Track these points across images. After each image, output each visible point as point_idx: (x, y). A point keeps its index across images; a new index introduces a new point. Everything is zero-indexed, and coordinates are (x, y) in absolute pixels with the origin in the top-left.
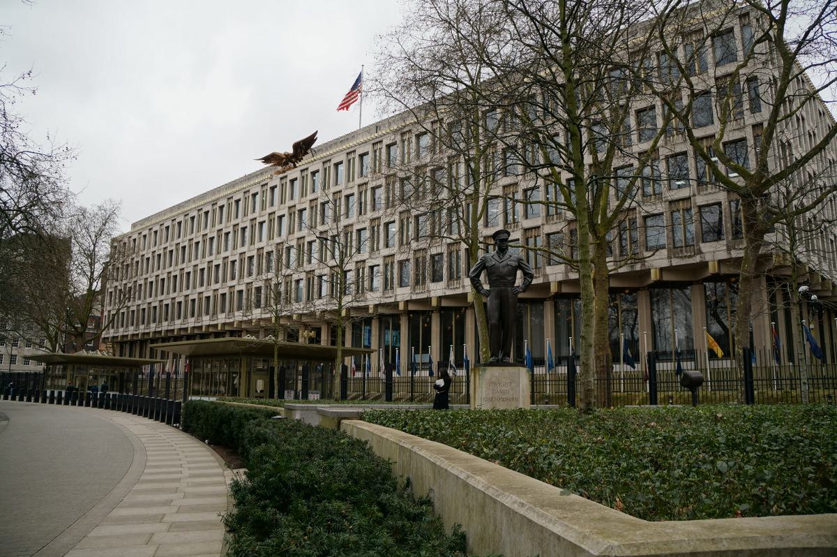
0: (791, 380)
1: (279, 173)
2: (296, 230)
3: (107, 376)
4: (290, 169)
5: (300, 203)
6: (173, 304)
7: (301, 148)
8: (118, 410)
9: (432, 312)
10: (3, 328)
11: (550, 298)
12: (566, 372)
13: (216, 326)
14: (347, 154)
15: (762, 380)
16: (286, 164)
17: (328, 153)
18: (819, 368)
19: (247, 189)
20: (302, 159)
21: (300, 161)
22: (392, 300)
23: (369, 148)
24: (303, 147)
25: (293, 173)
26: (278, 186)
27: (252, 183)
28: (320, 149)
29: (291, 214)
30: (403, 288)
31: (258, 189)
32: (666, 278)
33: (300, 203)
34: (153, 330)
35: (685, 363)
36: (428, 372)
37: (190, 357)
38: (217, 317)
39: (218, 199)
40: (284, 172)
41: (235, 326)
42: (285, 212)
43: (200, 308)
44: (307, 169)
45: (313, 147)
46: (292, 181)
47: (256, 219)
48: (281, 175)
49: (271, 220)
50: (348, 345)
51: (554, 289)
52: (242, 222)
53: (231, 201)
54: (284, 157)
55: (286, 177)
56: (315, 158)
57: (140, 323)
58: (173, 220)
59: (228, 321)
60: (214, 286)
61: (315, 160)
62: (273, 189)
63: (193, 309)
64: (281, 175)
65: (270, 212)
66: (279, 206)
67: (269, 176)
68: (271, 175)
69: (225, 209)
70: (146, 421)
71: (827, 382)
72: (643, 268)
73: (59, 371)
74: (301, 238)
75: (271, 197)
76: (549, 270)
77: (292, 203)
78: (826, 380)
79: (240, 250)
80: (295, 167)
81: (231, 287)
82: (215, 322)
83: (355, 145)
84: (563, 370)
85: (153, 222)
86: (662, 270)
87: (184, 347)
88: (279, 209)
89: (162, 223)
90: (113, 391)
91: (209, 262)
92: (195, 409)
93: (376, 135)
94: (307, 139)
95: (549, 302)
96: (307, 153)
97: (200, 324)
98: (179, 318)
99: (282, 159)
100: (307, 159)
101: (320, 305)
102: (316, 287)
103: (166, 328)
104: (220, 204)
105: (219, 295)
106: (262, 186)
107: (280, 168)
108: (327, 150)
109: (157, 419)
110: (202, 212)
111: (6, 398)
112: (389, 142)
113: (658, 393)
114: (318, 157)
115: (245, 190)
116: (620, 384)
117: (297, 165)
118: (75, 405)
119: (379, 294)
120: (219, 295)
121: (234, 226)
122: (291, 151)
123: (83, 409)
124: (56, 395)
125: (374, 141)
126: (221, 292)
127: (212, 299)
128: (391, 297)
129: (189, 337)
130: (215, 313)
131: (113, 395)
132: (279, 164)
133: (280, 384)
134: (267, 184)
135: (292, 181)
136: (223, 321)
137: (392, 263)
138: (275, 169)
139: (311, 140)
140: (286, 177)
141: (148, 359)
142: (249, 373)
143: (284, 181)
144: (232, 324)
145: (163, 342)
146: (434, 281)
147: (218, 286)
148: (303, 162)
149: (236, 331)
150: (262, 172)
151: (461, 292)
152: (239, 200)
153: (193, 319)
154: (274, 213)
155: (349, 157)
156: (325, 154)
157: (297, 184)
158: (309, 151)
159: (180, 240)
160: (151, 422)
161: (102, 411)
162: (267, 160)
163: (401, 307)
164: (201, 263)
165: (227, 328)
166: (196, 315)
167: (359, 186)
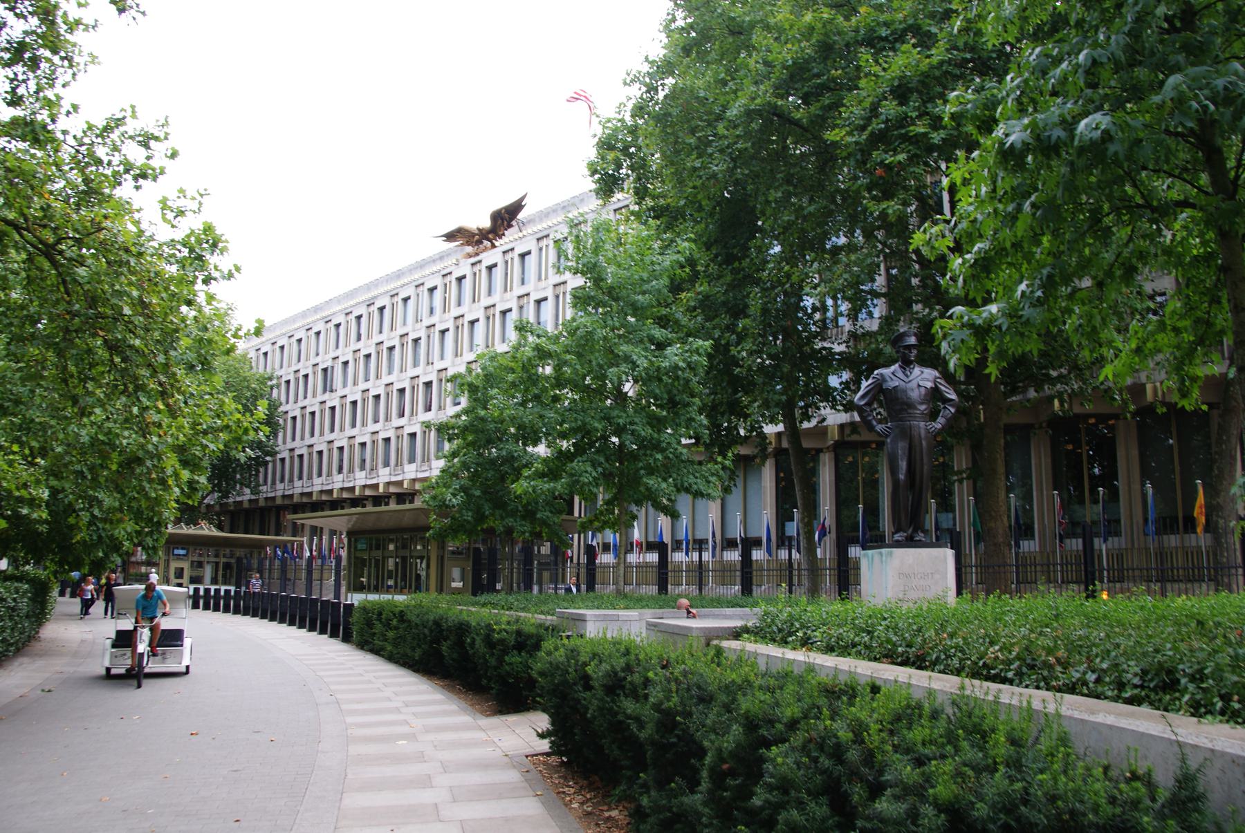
1: (470, 256)
2: (464, 351)
3: (217, 564)
4: (486, 249)
5: (502, 300)
6: (310, 454)
7: (502, 219)
8: (263, 617)
11: (828, 448)
13: (376, 486)
16: (479, 242)
17: (545, 226)
19: (420, 282)
20: (504, 234)
21: (500, 238)
24: (505, 218)
25: (489, 257)
27: (428, 272)
28: (531, 221)
29: (488, 318)
31: (437, 281)
33: (502, 300)
34: (279, 493)
36: (1080, 541)
37: (349, 534)
38: (377, 473)
39: (376, 297)
40: (477, 254)
41: (405, 486)
42: (480, 314)
43: (310, 467)
44: (512, 249)
45: (521, 216)
46: (490, 268)
47: (434, 325)
48: (473, 260)
49: (458, 327)
51: (834, 435)
52: (414, 331)
53: (395, 299)
54: (477, 232)
55: (480, 262)
56: (525, 233)
58: (308, 330)
59: (394, 479)
60: (397, 422)
61: (524, 236)
62: (460, 280)
63: (341, 460)
64: (473, 260)
65: (429, 324)
66: (413, 325)
67: (454, 261)
68: (457, 260)
69: (387, 312)
70: (293, 631)
73: (525, 526)
75: (457, 292)
77: (489, 302)
79: (412, 372)
80: (494, 246)
81: (350, 438)
82: (374, 481)
84: (1076, 544)
85: (278, 333)
87: (339, 521)
88: (470, 311)
89: (347, 311)
90: (225, 583)
91: (363, 391)
92: (372, 616)
93: (521, 235)
94: (511, 205)
95: (827, 455)
96: (510, 226)
97: (351, 485)
99: (473, 235)
100: (511, 235)
103: (319, 488)
104: (379, 304)
105: (357, 445)
106: (444, 276)
107: (469, 249)
108: (541, 220)
109: (312, 629)
110: (399, 299)
111: (814, 591)
112: (431, 286)
114: (530, 231)
115: (417, 283)
117: (497, 244)
118: (198, 608)
121: (401, 336)
122: (486, 223)
124: (202, 593)
126: (382, 435)
127: (346, 450)
129: (355, 502)
130: (399, 463)
131: (226, 591)
132: (468, 243)
133: (131, 580)
134: (450, 273)
135: (490, 268)
136: (387, 480)
138: (462, 250)
140: (480, 262)
142: (442, 558)
143: (476, 269)
144: (400, 483)
145: (332, 509)
147: (377, 427)
148: (505, 239)
150: (441, 257)
152: (384, 307)
153: (413, 466)
154: (463, 316)
156: (540, 227)
157: (498, 273)
158: (514, 223)
159: (299, 366)
160: (303, 632)
161: (239, 619)
162: (450, 237)
164: (375, 387)
165: (392, 490)
166: (286, 481)
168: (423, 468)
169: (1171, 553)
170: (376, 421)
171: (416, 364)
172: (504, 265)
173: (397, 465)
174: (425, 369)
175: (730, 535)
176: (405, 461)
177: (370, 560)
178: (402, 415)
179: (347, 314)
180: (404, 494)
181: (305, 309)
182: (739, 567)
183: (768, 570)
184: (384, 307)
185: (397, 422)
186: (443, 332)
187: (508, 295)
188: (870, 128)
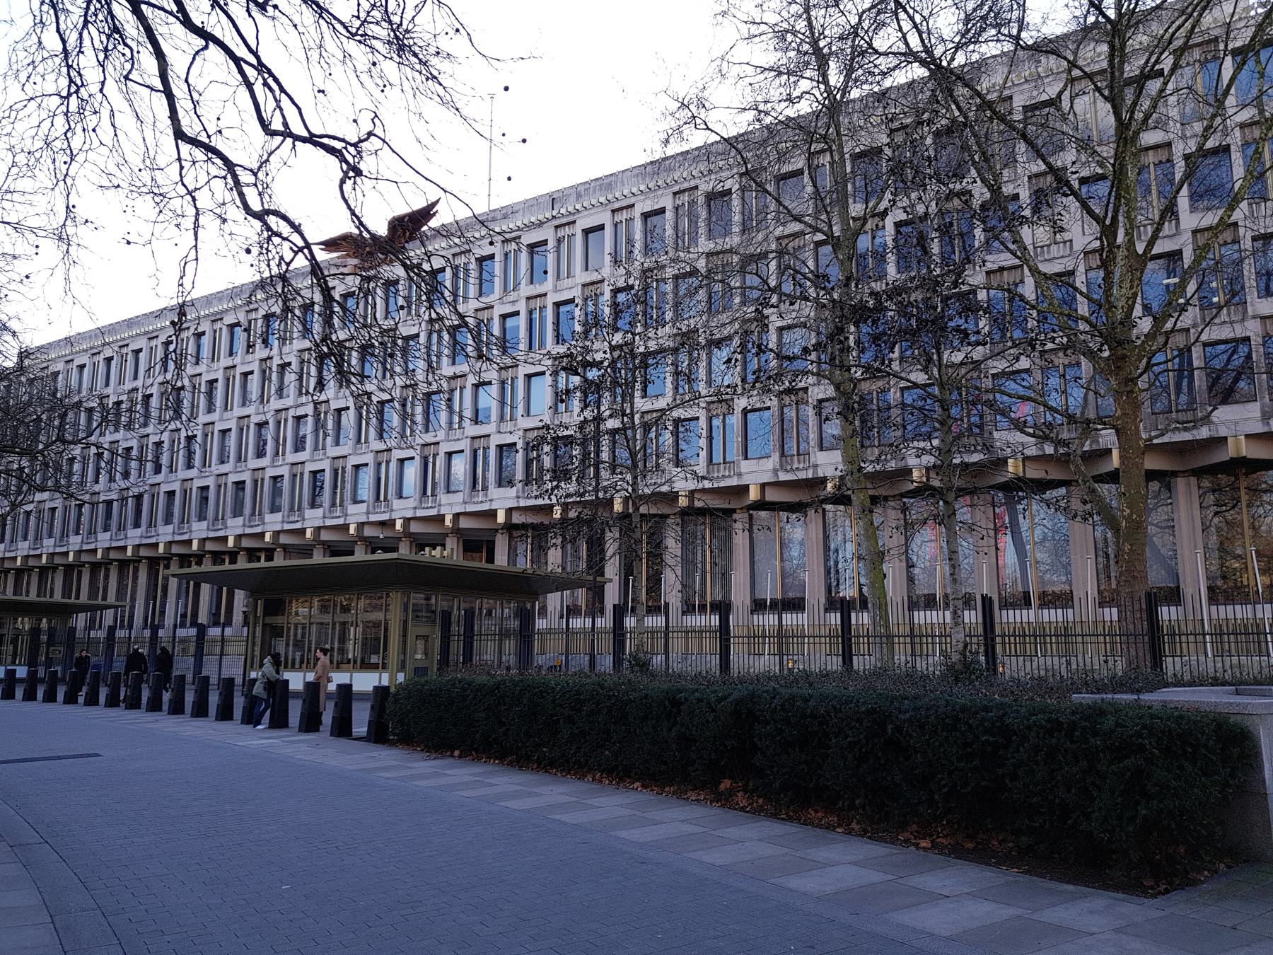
0: (1258, 634)
9: (447, 535)
10: (1266, 337)
12: (718, 624)
14: (613, 211)
15: (1195, 635)
18: (1078, 619)
19: (154, 334)
22: (433, 512)
23: (605, 218)
26: (207, 334)
30: (824, 453)
32: (772, 496)
35: (1165, 609)
36: (839, 615)
50: (111, 598)
53: (96, 358)
55: (157, 337)
57: (19, 538)
59: (58, 550)
60: (183, 474)
71: (1178, 640)
72: (1095, 447)
74: (244, 417)
75: (228, 338)
76: (745, 466)
78: (1226, 636)
83: (519, 229)
86: (763, 486)
98: (137, 525)
101: (402, 510)
102: (348, 486)
105: (162, 494)
113: (855, 658)
116: (764, 643)
119: (411, 503)
120: (230, 485)
123: (79, 711)
125: (213, 318)
128: (431, 507)
137: (486, 449)
139: (426, 213)
141: (84, 598)
146: (500, 484)
149: (101, 563)
151: (735, 484)
155: (617, 219)
163: (501, 518)
166: (176, 520)
167: (528, 299)
168: (292, 519)
169: (289, 629)
170: (189, 466)
171: (210, 410)
172: (212, 333)
173: (253, 514)
174: (221, 416)
175: (759, 596)
176: (129, 525)
177: (334, 624)
178: (189, 466)
179: (67, 362)
180: (159, 558)
181: (113, 321)
182: (194, 639)
183: (940, 636)
184: (84, 365)
185: (253, 463)
186: (245, 375)
187: (215, 365)
188: (847, 156)
